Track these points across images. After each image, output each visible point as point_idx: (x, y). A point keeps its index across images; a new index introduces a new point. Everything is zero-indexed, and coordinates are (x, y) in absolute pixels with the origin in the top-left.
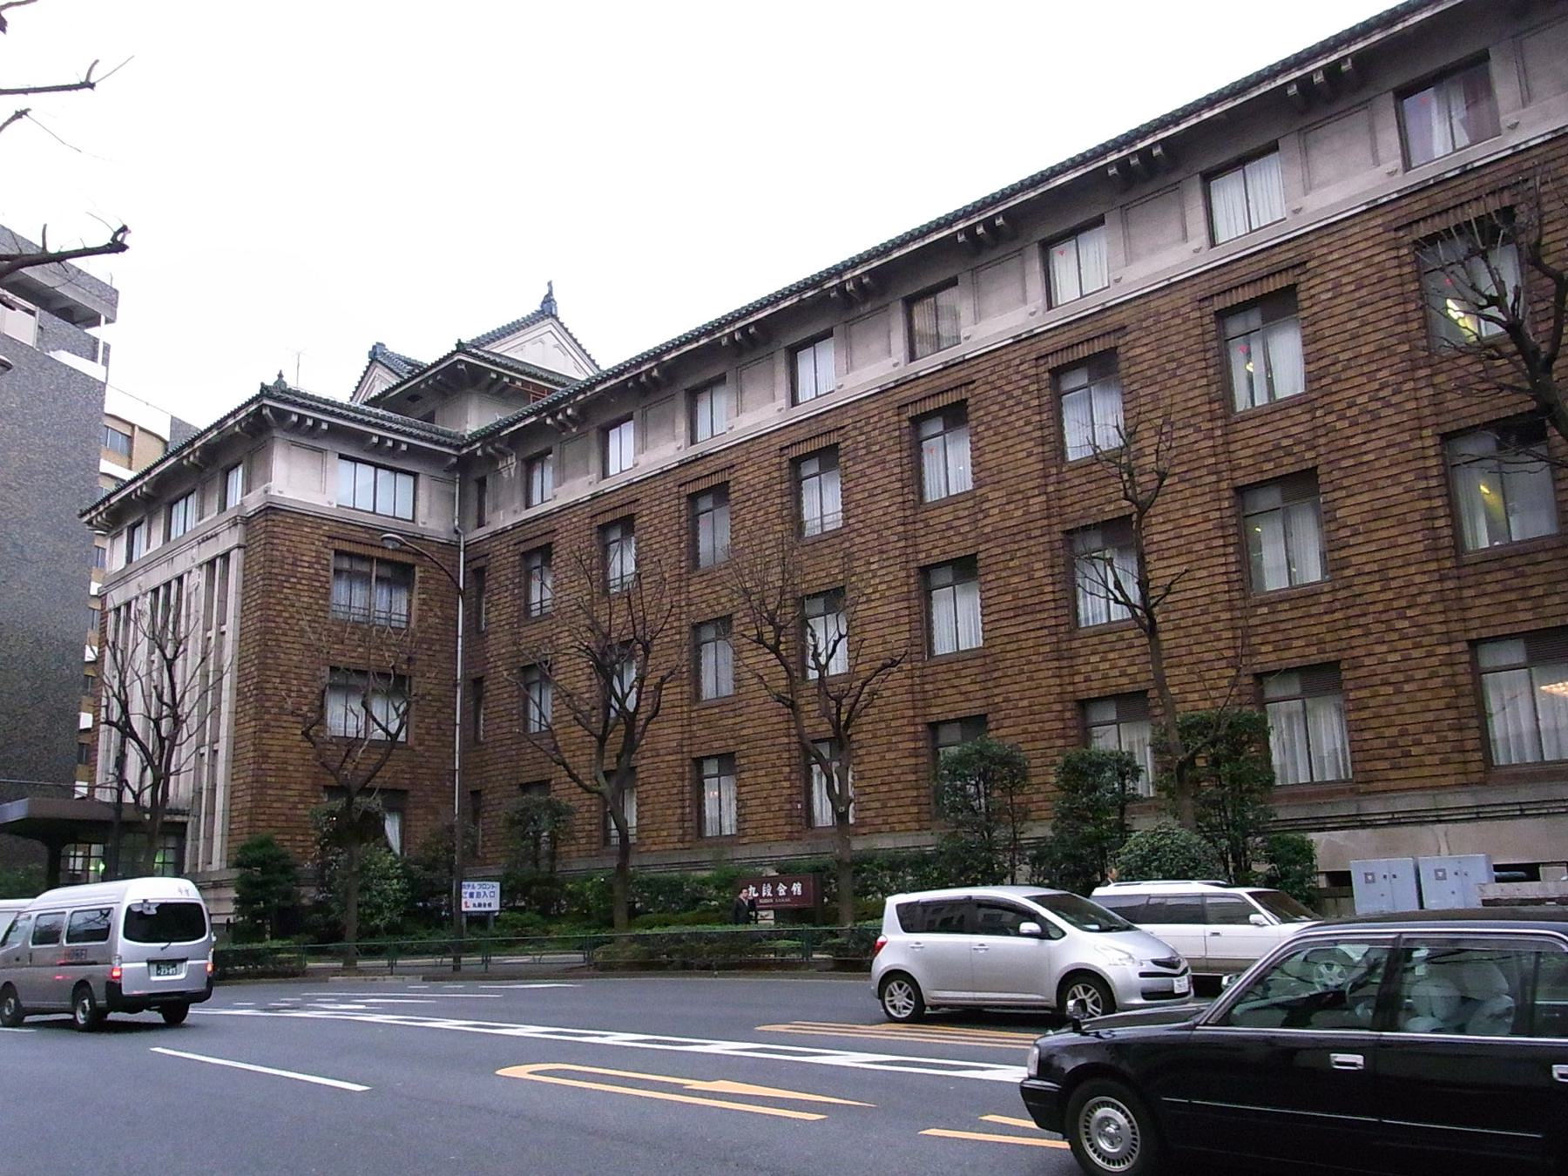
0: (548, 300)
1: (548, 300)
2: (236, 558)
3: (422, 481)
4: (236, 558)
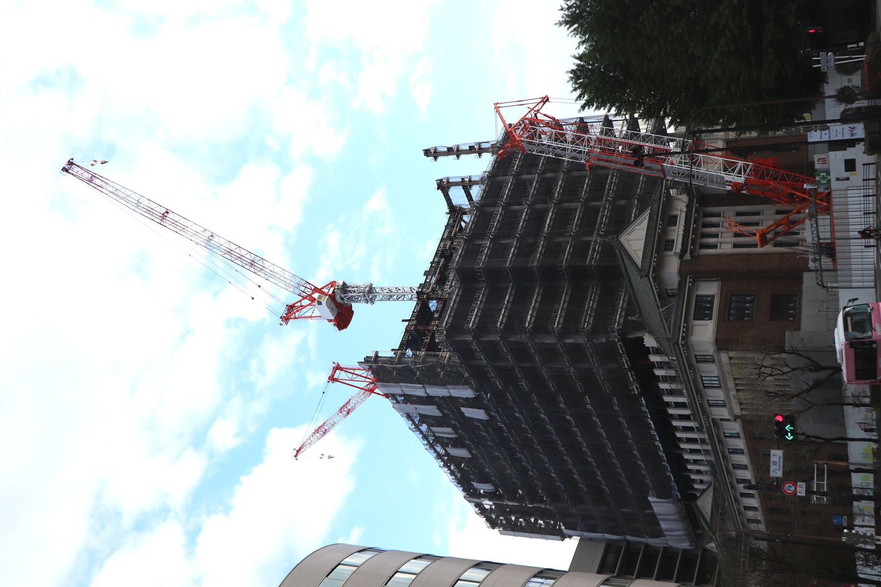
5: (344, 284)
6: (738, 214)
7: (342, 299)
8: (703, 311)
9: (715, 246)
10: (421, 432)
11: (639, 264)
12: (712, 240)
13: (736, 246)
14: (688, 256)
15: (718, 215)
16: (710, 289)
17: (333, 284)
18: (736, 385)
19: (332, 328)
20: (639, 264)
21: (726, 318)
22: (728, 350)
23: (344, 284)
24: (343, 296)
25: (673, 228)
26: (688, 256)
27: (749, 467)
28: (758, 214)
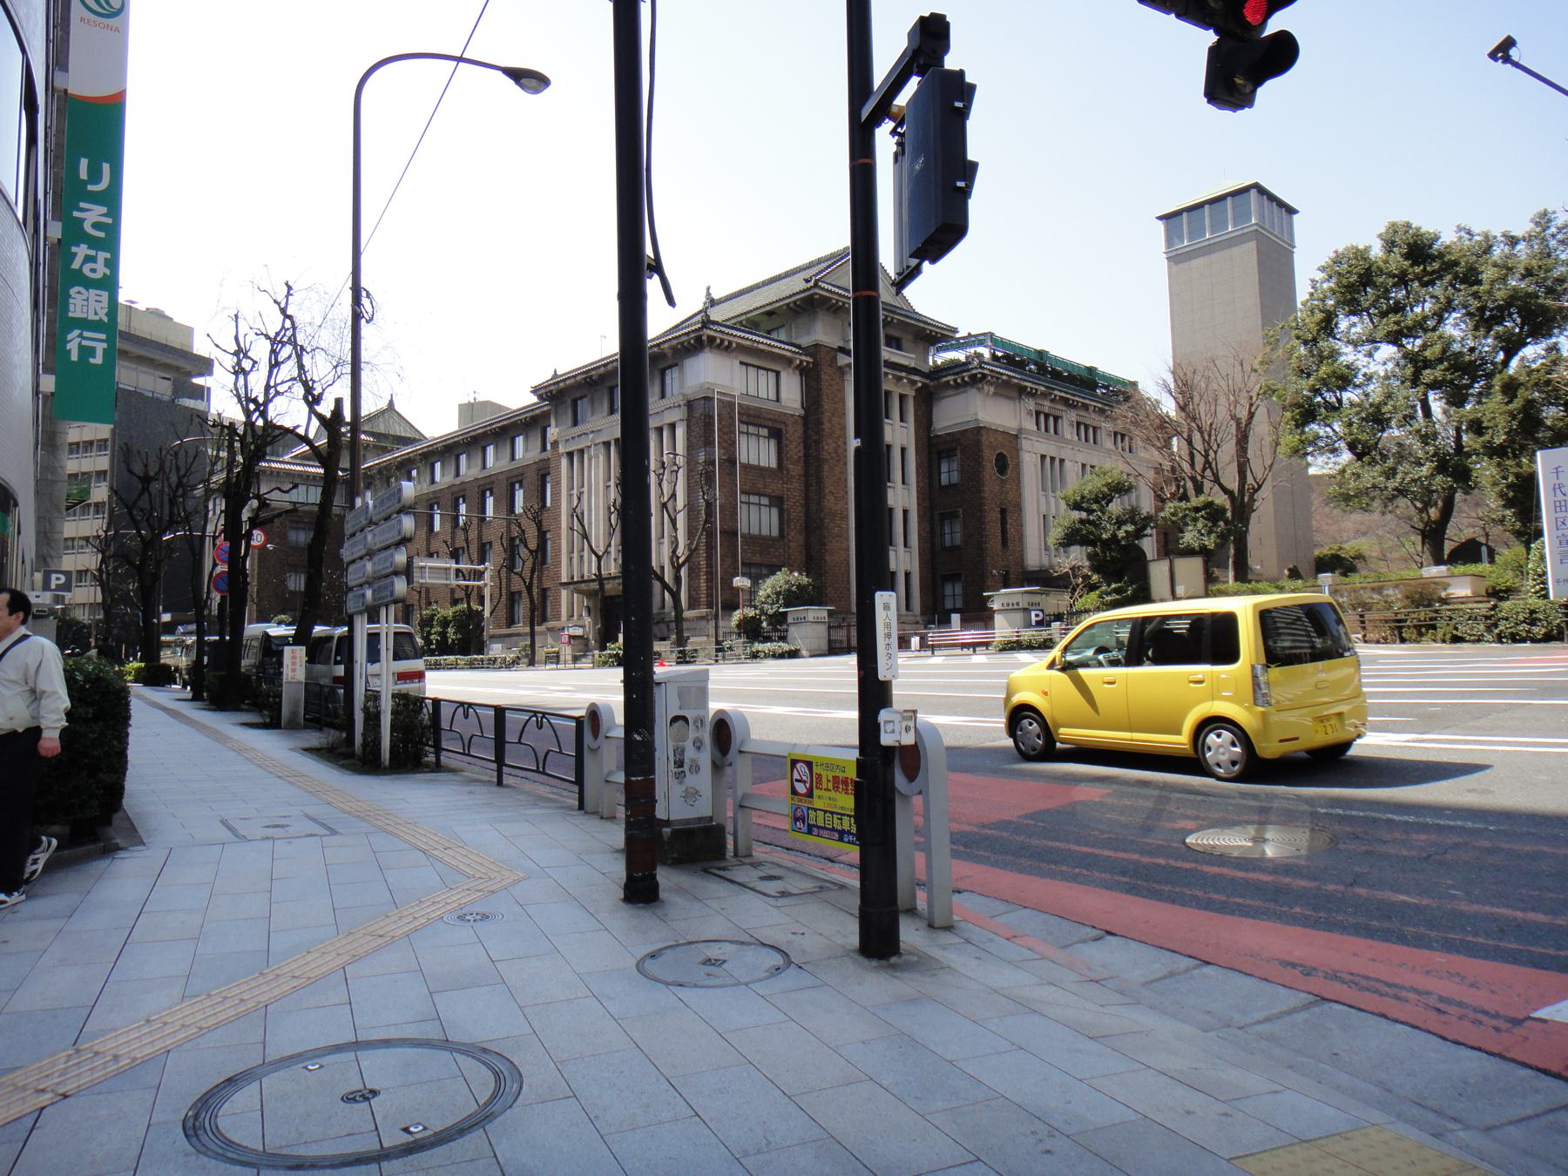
0: (391, 403)
1: (391, 403)
2: (680, 432)
3: (783, 375)
4: (680, 432)
22: (689, 421)
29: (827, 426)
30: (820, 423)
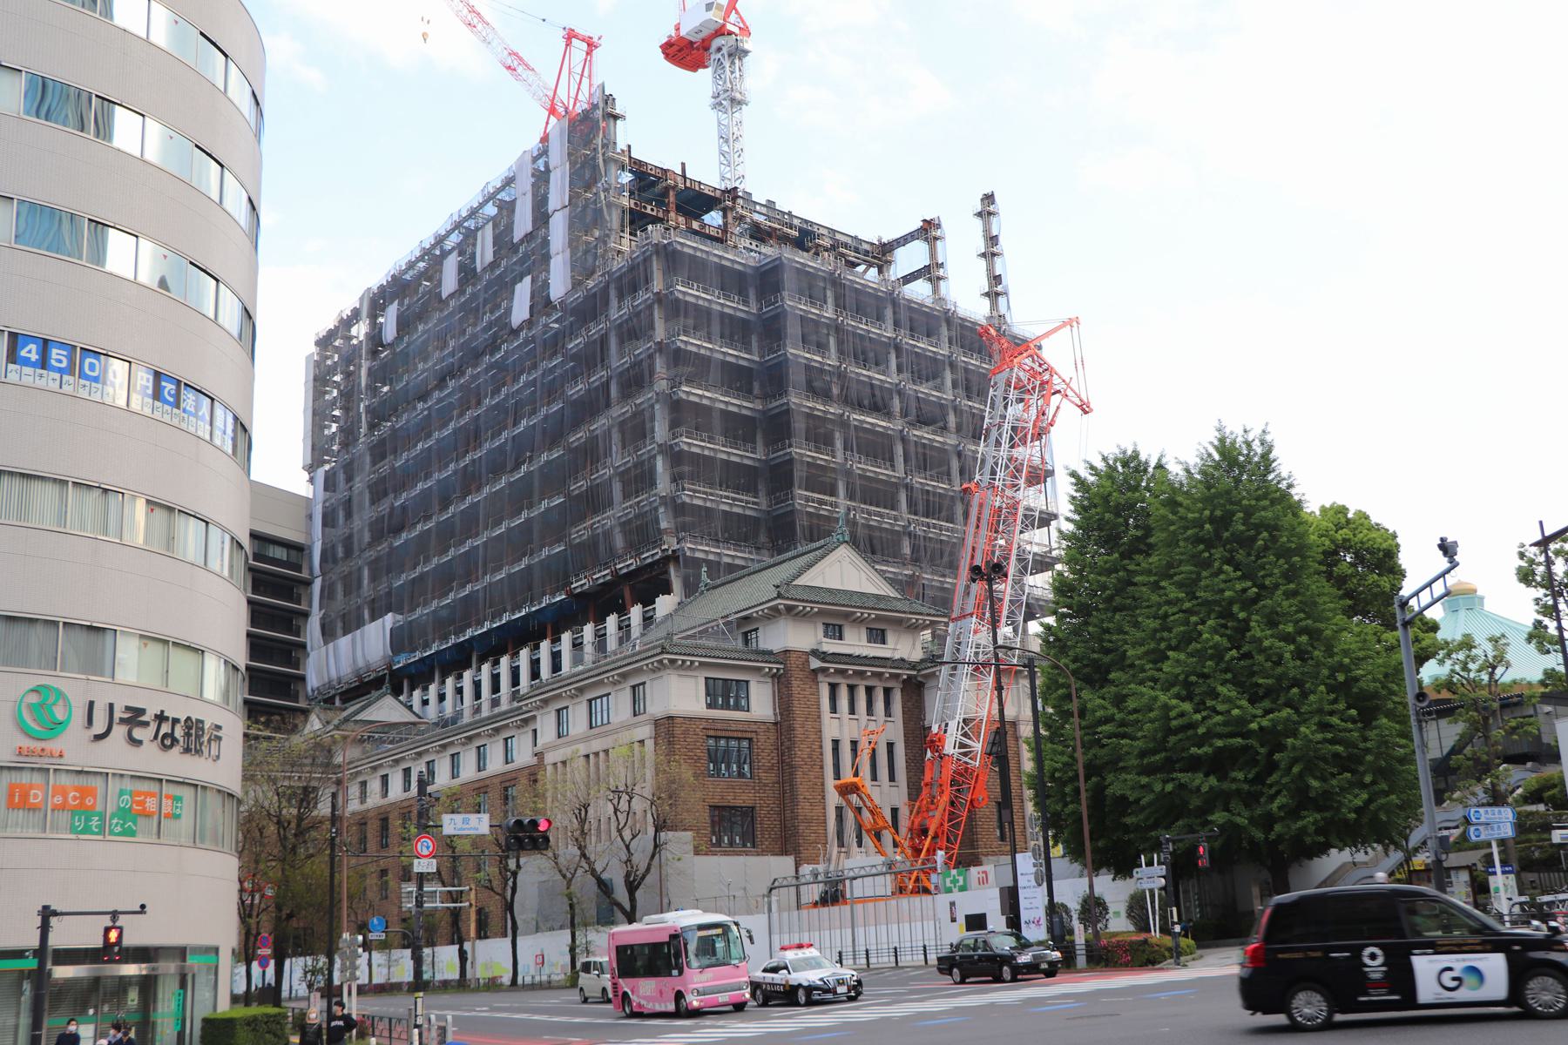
2: (650, 744)
5: (746, 52)
6: (890, 746)
7: (719, 49)
8: (723, 693)
9: (834, 709)
10: (481, 205)
11: (800, 581)
12: (843, 702)
13: (836, 743)
14: (815, 664)
15: (888, 713)
16: (761, 704)
17: (745, 31)
18: (596, 754)
19: (665, 33)
20: (800, 581)
21: (711, 733)
23: (746, 52)
24: (725, 51)
25: (864, 636)
26: (815, 664)
27: (457, 782)
28: (892, 778)
29: (799, 731)
30: (791, 729)
